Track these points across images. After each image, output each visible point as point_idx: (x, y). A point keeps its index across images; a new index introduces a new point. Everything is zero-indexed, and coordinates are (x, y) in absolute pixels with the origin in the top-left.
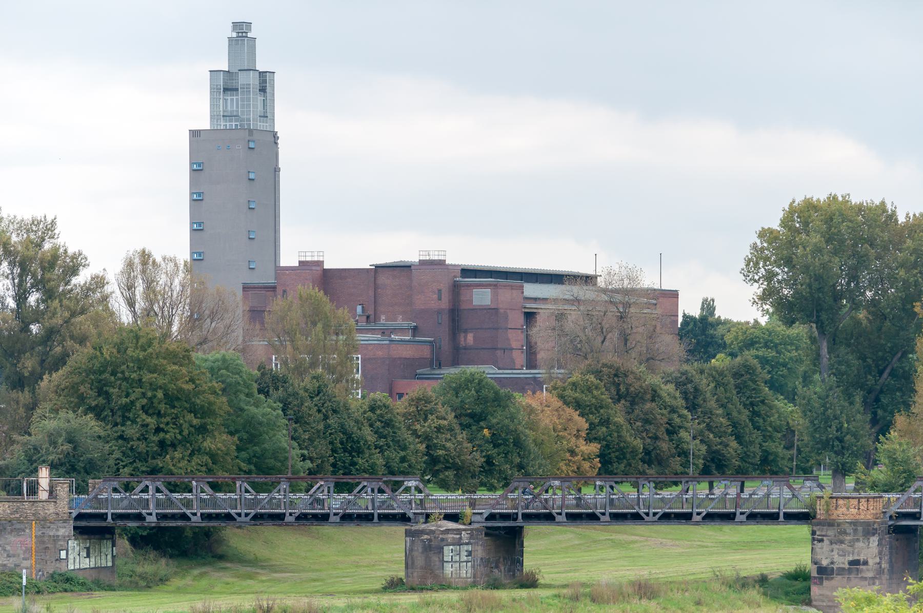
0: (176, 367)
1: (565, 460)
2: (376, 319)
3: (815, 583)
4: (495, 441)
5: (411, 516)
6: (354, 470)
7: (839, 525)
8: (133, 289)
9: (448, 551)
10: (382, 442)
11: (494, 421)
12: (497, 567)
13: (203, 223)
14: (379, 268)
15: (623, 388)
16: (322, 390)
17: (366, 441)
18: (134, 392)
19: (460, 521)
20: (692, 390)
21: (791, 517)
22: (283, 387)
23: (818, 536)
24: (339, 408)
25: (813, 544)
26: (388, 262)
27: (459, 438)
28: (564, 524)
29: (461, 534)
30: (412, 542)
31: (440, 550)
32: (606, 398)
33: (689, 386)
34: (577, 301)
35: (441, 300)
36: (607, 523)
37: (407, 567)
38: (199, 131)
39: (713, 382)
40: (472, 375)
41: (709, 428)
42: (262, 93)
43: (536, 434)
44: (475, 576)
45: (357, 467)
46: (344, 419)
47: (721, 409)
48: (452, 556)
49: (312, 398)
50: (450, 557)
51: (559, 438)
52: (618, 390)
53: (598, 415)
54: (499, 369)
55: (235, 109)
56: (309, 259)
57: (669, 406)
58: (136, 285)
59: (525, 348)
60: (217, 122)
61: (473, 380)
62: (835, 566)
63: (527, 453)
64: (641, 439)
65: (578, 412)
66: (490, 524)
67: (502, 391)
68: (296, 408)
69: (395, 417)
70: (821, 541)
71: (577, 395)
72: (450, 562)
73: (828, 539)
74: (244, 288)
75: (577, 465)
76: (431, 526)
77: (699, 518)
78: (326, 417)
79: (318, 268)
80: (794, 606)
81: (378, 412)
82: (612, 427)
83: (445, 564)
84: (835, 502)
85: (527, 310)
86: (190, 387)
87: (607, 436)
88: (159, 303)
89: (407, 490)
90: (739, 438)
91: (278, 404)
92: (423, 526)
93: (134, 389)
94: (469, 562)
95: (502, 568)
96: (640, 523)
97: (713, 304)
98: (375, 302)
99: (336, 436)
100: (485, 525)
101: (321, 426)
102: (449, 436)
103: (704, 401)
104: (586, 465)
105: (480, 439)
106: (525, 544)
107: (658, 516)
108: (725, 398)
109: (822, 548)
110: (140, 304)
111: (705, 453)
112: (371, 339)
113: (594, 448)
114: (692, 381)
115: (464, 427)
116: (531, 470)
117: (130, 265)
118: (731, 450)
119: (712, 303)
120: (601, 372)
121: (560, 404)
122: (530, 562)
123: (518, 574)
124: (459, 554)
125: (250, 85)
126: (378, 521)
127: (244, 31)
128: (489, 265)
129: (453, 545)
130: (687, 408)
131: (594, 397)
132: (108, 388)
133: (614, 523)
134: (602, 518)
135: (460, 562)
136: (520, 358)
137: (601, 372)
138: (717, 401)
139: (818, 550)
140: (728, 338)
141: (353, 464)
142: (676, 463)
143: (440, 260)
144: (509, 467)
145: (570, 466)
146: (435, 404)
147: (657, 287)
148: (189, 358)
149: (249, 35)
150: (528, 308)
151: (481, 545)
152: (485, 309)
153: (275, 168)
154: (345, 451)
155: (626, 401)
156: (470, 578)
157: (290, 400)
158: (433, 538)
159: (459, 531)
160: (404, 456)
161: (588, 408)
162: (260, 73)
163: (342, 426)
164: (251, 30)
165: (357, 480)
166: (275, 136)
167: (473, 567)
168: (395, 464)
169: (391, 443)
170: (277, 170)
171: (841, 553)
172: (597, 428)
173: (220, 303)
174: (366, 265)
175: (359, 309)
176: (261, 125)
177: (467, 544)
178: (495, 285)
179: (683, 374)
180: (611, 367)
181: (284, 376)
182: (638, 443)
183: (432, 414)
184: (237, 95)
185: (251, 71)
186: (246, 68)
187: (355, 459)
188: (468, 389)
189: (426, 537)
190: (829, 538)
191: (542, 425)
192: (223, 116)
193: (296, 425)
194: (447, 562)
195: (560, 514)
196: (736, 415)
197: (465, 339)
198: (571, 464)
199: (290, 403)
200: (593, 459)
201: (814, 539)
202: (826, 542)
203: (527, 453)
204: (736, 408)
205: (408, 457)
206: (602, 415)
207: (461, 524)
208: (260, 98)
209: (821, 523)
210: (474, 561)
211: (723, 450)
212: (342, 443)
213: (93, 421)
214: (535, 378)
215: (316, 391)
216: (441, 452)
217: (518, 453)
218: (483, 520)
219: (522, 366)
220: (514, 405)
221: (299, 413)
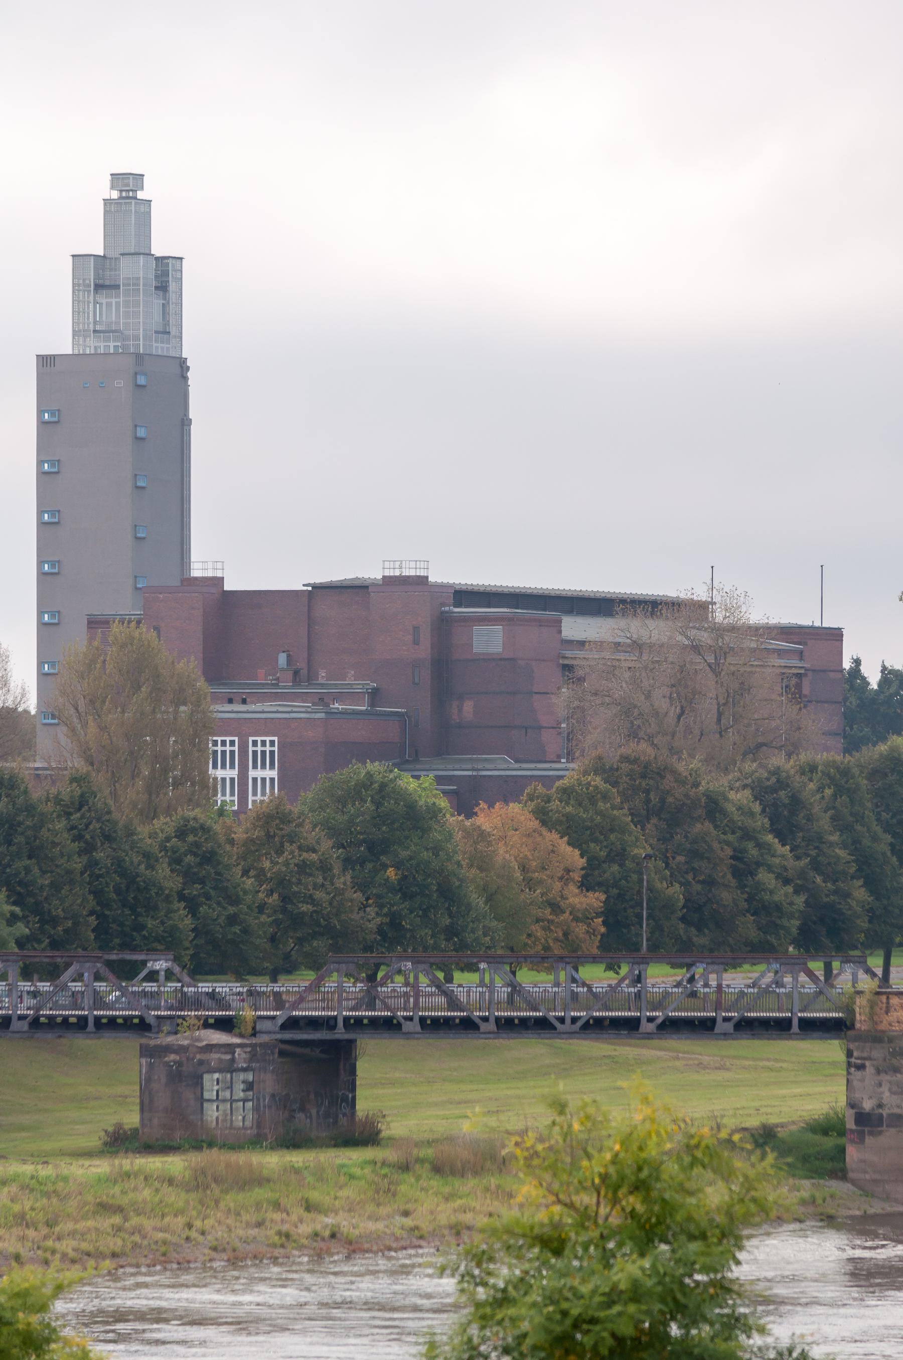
1: (543, 921)
2: (311, 678)
3: (852, 1141)
4: (404, 889)
5: (152, 1021)
6: (138, 938)
7: (891, 1040)
9: (211, 1083)
10: (195, 890)
11: (404, 854)
12: (302, 1109)
15: (654, 798)
16: (87, 801)
17: (161, 888)
19: (236, 1030)
20: (787, 801)
21: (811, 1027)
22: (8, 796)
23: (856, 1058)
24: (115, 832)
25: (849, 1073)
27: (339, 883)
28: (416, 1036)
29: (234, 1052)
30: (151, 1066)
31: (197, 1081)
32: (623, 816)
33: (782, 793)
34: (637, 646)
36: (491, 1036)
37: (142, 1111)
39: (830, 788)
41: (816, 866)
42: (161, 293)
43: (487, 876)
44: (259, 1124)
45: (145, 932)
46: (124, 851)
48: (218, 1092)
50: (215, 1093)
51: (530, 884)
52: (648, 801)
53: (605, 843)
54: (516, 762)
55: (114, 319)
57: (739, 828)
60: (85, 341)
62: (885, 1112)
63: (463, 908)
64: (681, 884)
66: (288, 1035)
69: (220, 846)
70: (861, 1067)
71: (569, 809)
72: (213, 1101)
73: (873, 1066)
74: (90, 622)
75: (563, 930)
76: (182, 1040)
77: (651, 1027)
78: (89, 849)
79: (213, 590)
80: (813, 1181)
81: (191, 838)
82: (629, 864)
83: (205, 1105)
84: (884, 1000)
87: (620, 880)
89: (152, 976)
90: (872, 884)
92: (170, 1039)
94: (248, 1100)
95: (314, 1112)
96: (548, 1036)
98: (309, 648)
99: (108, 880)
100: (279, 1036)
101: (78, 864)
102: (320, 880)
103: (808, 820)
104: (580, 929)
105: (380, 885)
106: (359, 1072)
107: (579, 1024)
108: (851, 814)
109: (862, 1080)
111: (802, 908)
112: (281, 709)
113: (595, 900)
114: (788, 785)
115: (348, 863)
116: (469, 937)
118: (854, 904)
120: (617, 769)
121: (535, 824)
122: (364, 1105)
123: (343, 1121)
124: (231, 1088)
125: (138, 279)
126: (94, 1030)
127: (131, 187)
129: (220, 1071)
130: (771, 832)
131: (601, 813)
133: (504, 1035)
134: (484, 1027)
135: (232, 1101)
137: (617, 769)
138: (833, 819)
139: (855, 1083)
141: (138, 928)
142: (748, 926)
144: (430, 933)
145: (551, 930)
146: (298, 826)
147: (817, 624)
149: (140, 195)
151: (273, 1071)
152: (494, 659)
154: (124, 906)
155: (660, 819)
156: (252, 1128)
157: (20, 818)
158: (184, 1059)
159: (230, 1048)
160: (235, 914)
161: (588, 832)
162: (157, 259)
163: (119, 864)
165: (67, 960)
166: (182, 366)
167: (256, 1109)
168: (218, 928)
169: (212, 893)
170: (185, 423)
171: (895, 1089)
172: (604, 865)
174: (296, 584)
175: (282, 659)
176: (159, 348)
177: (244, 1070)
180: (635, 761)
182: (676, 891)
183: (292, 842)
184: (118, 296)
185: (142, 256)
186: (133, 251)
187: (141, 919)
189: (172, 1057)
190: (875, 1062)
191: (499, 860)
192: (95, 331)
193: (28, 862)
194: (209, 1100)
195: (410, 1019)
196: (869, 844)
197: (460, 710)
198: (552, 927)
199: (20, 824)
200: (592, 919)
201: (849, 1065)
202: (870, 1070)
203: (463, 908)
204: (869, 830)
205: (241, 916)
206: (612, 844)
207: (236, 1035)
208: (158, 302)
209: (860, 1038)
210: (258, 1099)
211: (840, 903)
212: (118, 891)
215: (77, 803)
216: (305, 908)
217: (448, 909)
218: (277, 1029)
219: (559, 757)
221: (35, 840)
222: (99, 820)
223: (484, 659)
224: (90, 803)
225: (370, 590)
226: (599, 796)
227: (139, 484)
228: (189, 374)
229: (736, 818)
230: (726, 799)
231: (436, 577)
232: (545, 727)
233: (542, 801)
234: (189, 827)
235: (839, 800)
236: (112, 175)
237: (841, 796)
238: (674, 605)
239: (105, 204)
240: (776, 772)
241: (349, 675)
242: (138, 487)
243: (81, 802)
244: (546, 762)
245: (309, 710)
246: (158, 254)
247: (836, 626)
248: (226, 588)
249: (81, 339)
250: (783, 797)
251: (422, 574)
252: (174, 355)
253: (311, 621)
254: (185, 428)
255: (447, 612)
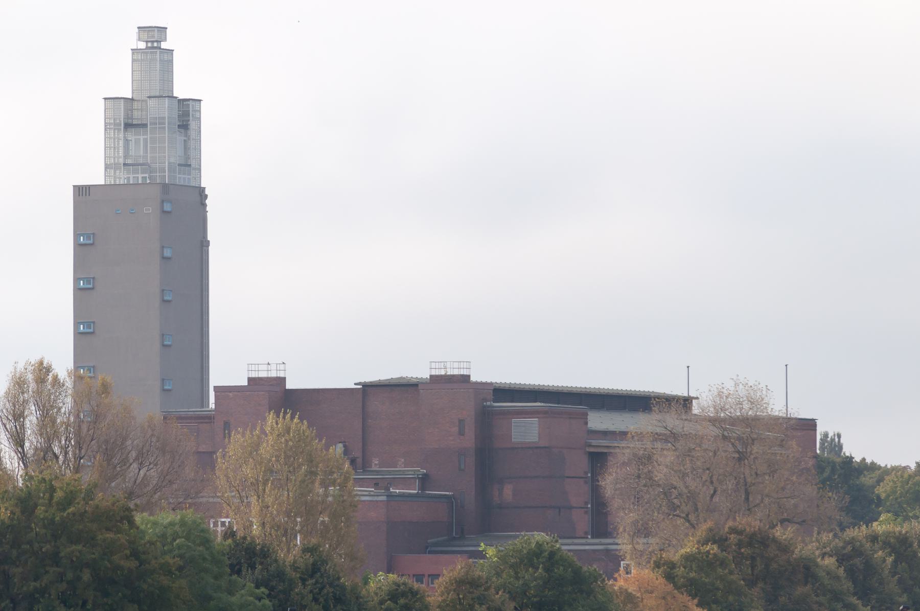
0: (110, 535)
8: (22, 420)
13: (94, 323)
14: (368, 389)
18: (47, 572)
22: (261, 563)
26: (394, 377)
35: (463, 435)
38: (88, 188)
40: (539, 545)
42: (182, 131)
47: (905, 595)
49: (303, 581)
55: (142, 153)
56: (263, 374)
58: (26, 413)
59: (589, 506)
60: (115, 173)
61: (541, 554)
65: (696, 601)
67: (585, 569)
68: (281, 596)
71: (692, 575)
85: (592, 450)
86: (132, 564)
88: (60, 442)
91: (263, 589)
93: (48, 568)
97: (839, 441)
98: (363, 438)
110: (31, 441)
117: (19, 383)
119: (837, 440)
128: (532, 383)
130: (855, 594)
132: (6, 567)
136: (582, 521)
138: (900, 581)
140: (882, 491)
143: (463, 376)
148: (131, 522)
149: (164, 45)
150: (594, 446)
152: (529, 448)
153: (202, 242)
162: (180, 101)
164: (166, 39)
166: (201, 195)
170: (204, 244)
173: (154, 439)
174: (348, 382)
176: (181, 179)
178: (546, 413)
179: (849, 543)
181: (263, 547)
186: (158, 94)
188: (532, 566)
192: (125, 164)
208: (180, 138)
213: (274, 584)
214: (608, 551)
219: (586, 533)
220: (602, 589)
222: (331, 585)
223: (522, 448)
224: (322, 570)
225: (419, 388)
226: (718, 563)
227: (166, 298)
228: (207, 202)
229: (826, 582)
230: (817, 565)
231: (477, 377)
232: (576, 508)
233: (668, 567)
234: (400, 590)
235: (900, 566)
236: (139, 28)
237: (901, 563)
238: (668, 402)
239: (133, 54)
240: (852, 541)
241: (400, 463)
242: (164, 301)
243: (314, 569)
244: (576, 538)
245: (372, 493)
246: (181, 97)
247: (811, 418)
248: (287, 388)
249: (112, 171)
250: (859, 563)
251: (465, 373)
252: (194, 185)
253: (365, 416)
254: (204, 248)
255: (489, 407)
